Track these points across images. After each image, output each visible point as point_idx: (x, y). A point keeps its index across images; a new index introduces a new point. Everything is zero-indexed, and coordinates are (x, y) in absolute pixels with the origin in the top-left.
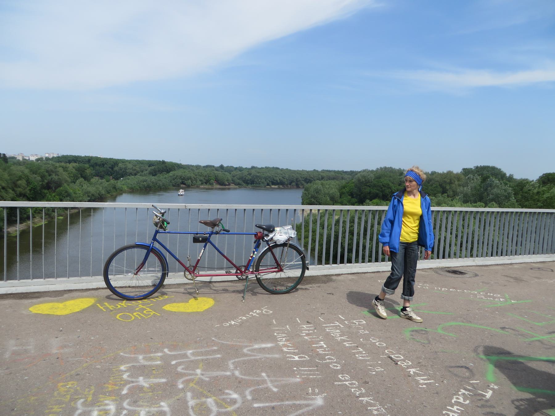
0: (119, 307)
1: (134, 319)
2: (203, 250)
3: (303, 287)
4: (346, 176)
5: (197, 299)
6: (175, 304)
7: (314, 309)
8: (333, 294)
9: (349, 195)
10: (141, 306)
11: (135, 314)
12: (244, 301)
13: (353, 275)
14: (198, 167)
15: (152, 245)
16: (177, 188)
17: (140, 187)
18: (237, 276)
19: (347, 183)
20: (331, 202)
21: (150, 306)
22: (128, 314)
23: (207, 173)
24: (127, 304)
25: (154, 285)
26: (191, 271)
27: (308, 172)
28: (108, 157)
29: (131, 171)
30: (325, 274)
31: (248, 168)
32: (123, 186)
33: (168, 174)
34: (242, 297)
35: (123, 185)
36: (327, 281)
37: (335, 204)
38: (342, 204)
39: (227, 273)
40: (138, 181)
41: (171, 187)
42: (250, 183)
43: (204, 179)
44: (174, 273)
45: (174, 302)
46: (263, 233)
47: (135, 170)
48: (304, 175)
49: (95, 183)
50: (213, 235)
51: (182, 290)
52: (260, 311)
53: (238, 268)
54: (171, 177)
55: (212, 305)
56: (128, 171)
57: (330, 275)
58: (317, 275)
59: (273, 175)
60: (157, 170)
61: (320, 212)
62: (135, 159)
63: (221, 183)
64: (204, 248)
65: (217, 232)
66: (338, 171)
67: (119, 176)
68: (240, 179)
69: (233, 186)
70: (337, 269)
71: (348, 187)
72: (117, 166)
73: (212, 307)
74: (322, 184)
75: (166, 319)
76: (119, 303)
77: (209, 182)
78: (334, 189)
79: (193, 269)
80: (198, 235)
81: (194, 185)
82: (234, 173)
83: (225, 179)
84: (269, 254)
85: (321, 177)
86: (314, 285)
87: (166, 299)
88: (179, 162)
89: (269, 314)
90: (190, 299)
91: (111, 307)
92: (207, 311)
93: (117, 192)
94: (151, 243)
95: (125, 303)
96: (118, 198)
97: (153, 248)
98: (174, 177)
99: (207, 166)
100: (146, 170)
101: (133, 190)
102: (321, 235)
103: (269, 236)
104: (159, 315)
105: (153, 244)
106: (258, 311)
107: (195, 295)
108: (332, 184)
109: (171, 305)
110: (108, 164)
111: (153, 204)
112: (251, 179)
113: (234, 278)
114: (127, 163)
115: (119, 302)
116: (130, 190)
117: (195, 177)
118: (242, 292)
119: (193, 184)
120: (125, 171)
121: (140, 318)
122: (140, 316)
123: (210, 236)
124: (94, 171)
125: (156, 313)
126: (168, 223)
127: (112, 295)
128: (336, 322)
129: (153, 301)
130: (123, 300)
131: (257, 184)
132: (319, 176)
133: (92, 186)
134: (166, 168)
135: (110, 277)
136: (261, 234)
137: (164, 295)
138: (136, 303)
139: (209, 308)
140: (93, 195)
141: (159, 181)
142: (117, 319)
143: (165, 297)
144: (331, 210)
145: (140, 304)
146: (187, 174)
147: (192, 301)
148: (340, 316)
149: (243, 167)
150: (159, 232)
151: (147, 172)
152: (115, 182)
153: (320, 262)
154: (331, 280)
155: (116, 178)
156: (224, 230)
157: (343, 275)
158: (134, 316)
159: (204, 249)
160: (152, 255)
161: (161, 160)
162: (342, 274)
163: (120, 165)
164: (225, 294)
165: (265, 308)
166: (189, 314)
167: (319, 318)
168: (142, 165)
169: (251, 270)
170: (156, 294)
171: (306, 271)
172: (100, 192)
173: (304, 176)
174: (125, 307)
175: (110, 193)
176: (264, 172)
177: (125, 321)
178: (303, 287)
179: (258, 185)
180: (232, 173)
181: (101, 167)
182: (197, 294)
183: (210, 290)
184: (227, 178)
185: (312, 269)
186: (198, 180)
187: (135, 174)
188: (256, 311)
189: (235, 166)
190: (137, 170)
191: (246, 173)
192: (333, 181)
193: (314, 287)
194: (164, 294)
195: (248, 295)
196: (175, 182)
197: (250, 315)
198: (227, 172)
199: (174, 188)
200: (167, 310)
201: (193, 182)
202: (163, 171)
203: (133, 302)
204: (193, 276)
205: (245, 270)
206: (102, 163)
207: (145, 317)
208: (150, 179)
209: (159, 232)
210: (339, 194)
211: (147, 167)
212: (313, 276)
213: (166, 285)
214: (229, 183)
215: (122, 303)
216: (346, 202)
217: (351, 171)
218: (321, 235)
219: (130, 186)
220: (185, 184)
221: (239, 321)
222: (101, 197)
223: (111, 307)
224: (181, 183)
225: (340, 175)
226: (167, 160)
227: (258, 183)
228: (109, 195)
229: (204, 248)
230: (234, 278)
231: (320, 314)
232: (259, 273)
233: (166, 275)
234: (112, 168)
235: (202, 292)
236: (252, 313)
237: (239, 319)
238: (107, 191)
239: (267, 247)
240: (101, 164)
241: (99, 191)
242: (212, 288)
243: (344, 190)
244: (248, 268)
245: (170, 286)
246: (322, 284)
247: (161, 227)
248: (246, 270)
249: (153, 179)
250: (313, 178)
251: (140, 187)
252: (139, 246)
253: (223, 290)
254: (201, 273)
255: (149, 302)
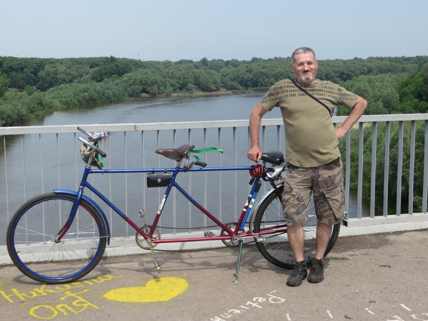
0: (35, 295)
1: (57, 316)
2: (164, 199)
3: (339, 255)
4: (409, 66)
5: (160, 281)
6: (124, 289)
7: (357, 293)
8: (389, 267)
9: (416, 97)
10: (69, 294)
11: (58, 307)
12: (236, 281)
13: (424, 232)
14: (167, 64)
15: (80, 193)
16: (136, 99)
17: (79, 101)
18: (223, 240)
19: (411, 77)
20: (387, 110)
21: (83, 293)
22: (48, 307)
23: (182, 72)
24: (47, 291)
25: (90, 258)
26: (147, 234)
27: (345, 62)
28: (29, 56)
29: (64, 76)
30: (376, 232)
31: (247, 61)
32: (53, 100)
33: (120, 78)
34: (234, 275)
35: (54, 98)
36: (380, 244)
37: (392, 112)
38: (403, 111)
39: (207, 236)
40: (75, 91)
41: (127, 98)
42: (251, 85)
43: (178, 82)
44: (122, 238)
45: (123, 285)
46: (264, 167)
47: (70, 74)
48: (338, 67)
49: (13, 98)
50: (179, 173)
51: (135, 265)
52: (264, 300)
53: (225, 228)
54: (126, 82)
55: (184, 290)
56: (59, 77)
57: (384, 234)
58: (361, 234)
59: (287, 69)
60: (104, 72)
61: (364, 126)
62: (69, 57)
63: (204, 88)
64: (165, 196)
65: (186, 167)
66: (396, 58)
67: (46, 85)
68: (234, 79)
69: (224, 91)
70: (397, 222)
71: (413, 84)
72: (43, 70)
73: (184, 293)
74: (370, 82)
75: (108, 315)
76: (35, 289)
77: (185, 86)
78: (389, 89)
79: (149, 230)
80: (155, 174)
81: (163, 93)
82: (225, 70)
83: (211, 82)
84: (276, 202)
85: (368, 69)
86: (357, 252)
87: (109, 281)
88: (136, 58)
89: (279, 303)
90: (148, 280)
91: (21, 296)
92: (175, 300)
93: (44, 109)
94: (79, 189)
95: (45, 289)
96: (47, 119)
97: (82, 197)
98: (131, 81)
99: (181, 62)
100: (87, 74)
101: (69, 106)
102: (368, 164)
103: (274, 170)
104: (97, 308)
105: (82, 192)
106: (260, 300)
107: (156, 274)
108: (386, 79)
109: (118, 290)
110: (29, 68)
111: (79, 126)
112: (252, 79)
113: (219, 244)
114: (58, 64)
115: (36, 288)
116: (64, 107)
117: (163, 80)
118: (229, 266)
119: (160, 92)
120: (55, 77)
121: (66, 314)
122: (66, 310)
123: (175, 175)
124: (9, 80)
125: (92, 305)
126: (104, 156)
127: (21, 276)
128: (395, 316)
129: (89, 284)
130: (42, 284)
131: (263, 86)
132: (364, 68)
133: (7, 103)
134: (118, 67)
135: (17, 247)
136: (261, 169)
137: (106, 274)
138: (62, 288)
139: (179, 295)
140: (9, 116)
141: (107, 89)
142: (30, 316)
143: (108, 278)
144: (383, 122)
145: (68, 290)
146: (152, 76)
147: (151, 283)
148: (403, 305)
149: (239, 60)
150: (90, 171)
151: (89, 76)
152: (41, 95)
153: (366, 213)
154: (387, 243)
155: (41, 88)
156: (197, 164)
157: (407, 233)
158: (57, 310)
159: (166, 198)
160: (81, 211)
161: (109, 56)
162: (405, 232)
163: (47, 67)
164: (207, 271)
165: (273, 294)
166: (146, 305)
167: (367, 309)
168: (80, 66)
169: (246, 229)
170: (92, 273)
171: (342, 228)
172: (19, 111)
173: (338, 69)
174: (44, 296)
175: (35, 113)
176: (273, 67)
177: (43, 318)
178: (339, 255)
179: (264, 88)
180: (221, 70)
181: (18, 72)
182: (159, 271)
183: (182, 264)
184: (214, 79)
185: (354, 225)
186: (168, 85)
187: (71, 81)
188: (257, 300)
189: (225, 60)
190: (72, 74)
191: (243, 69)
192: (386, 74)
193: (357, 255)
194: (105, 272)
195: (243, 272)
196: (132, 89)
197: (246, 306)
198: (214, 69)
199: (131, 99)
200: (110, 301)
201: (160, 88)
202: (113, 74)
203: (58, 287)
204: (150, 243)
205: (237, 230)
206: (20, 65)
207: (74, 311)
208: (93, 87)
209: (90, 171)
210: (398, 95)
211: (88, 69)
212: (355, 236)
213: (111, 257)
214: (217, 87)
215: (39, 289)
216: (411, 109)
217: (417, 57)
218: (368, 164)
219: (64, 99)
220: (147, 92)
221: (229, 317)
222: (21, 119)
223: (21, 296)
224: (141, 91)
225: (399, 64)
226: (118, 55)
227: (264, 85)
228: (33, 116)
229: (165, 196)
230: (219, 244)
231: (368, 303)
232: (260, 235)
233: (107, 243)
234: (35, 74)
235: (168, 267)
236: (251, 303)
237: (229, 313)
238: (30, 109)
239: (272, 190)
240: (19, 68)
241: (18, 110)
242: (184, 260)
243: (406, 89)
244: (241, 226)
245: (117, 259)
246: (371, 249)
247: (94, 163)
248: (238, 230)
249: (99, 86)
250: (354, 72)
251: (79, 101)
252: (59, 195)
253: (203, 264)
254: (164, 236)
255: (83, 286)
